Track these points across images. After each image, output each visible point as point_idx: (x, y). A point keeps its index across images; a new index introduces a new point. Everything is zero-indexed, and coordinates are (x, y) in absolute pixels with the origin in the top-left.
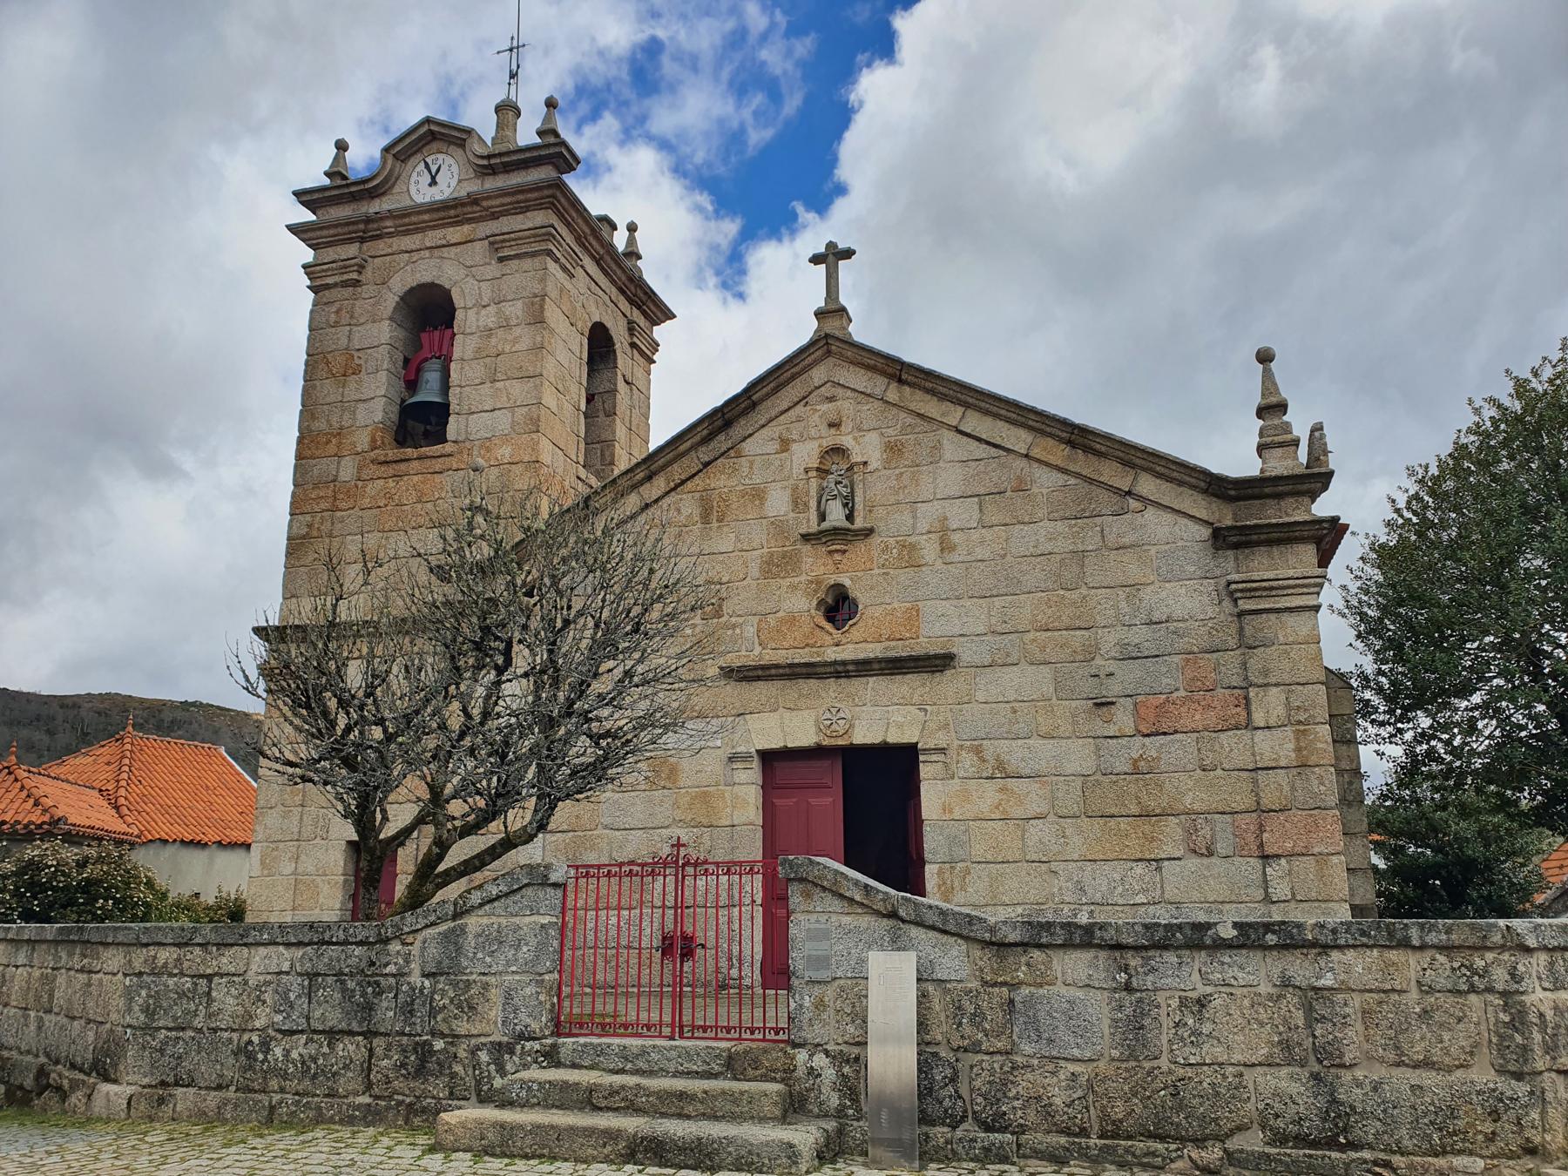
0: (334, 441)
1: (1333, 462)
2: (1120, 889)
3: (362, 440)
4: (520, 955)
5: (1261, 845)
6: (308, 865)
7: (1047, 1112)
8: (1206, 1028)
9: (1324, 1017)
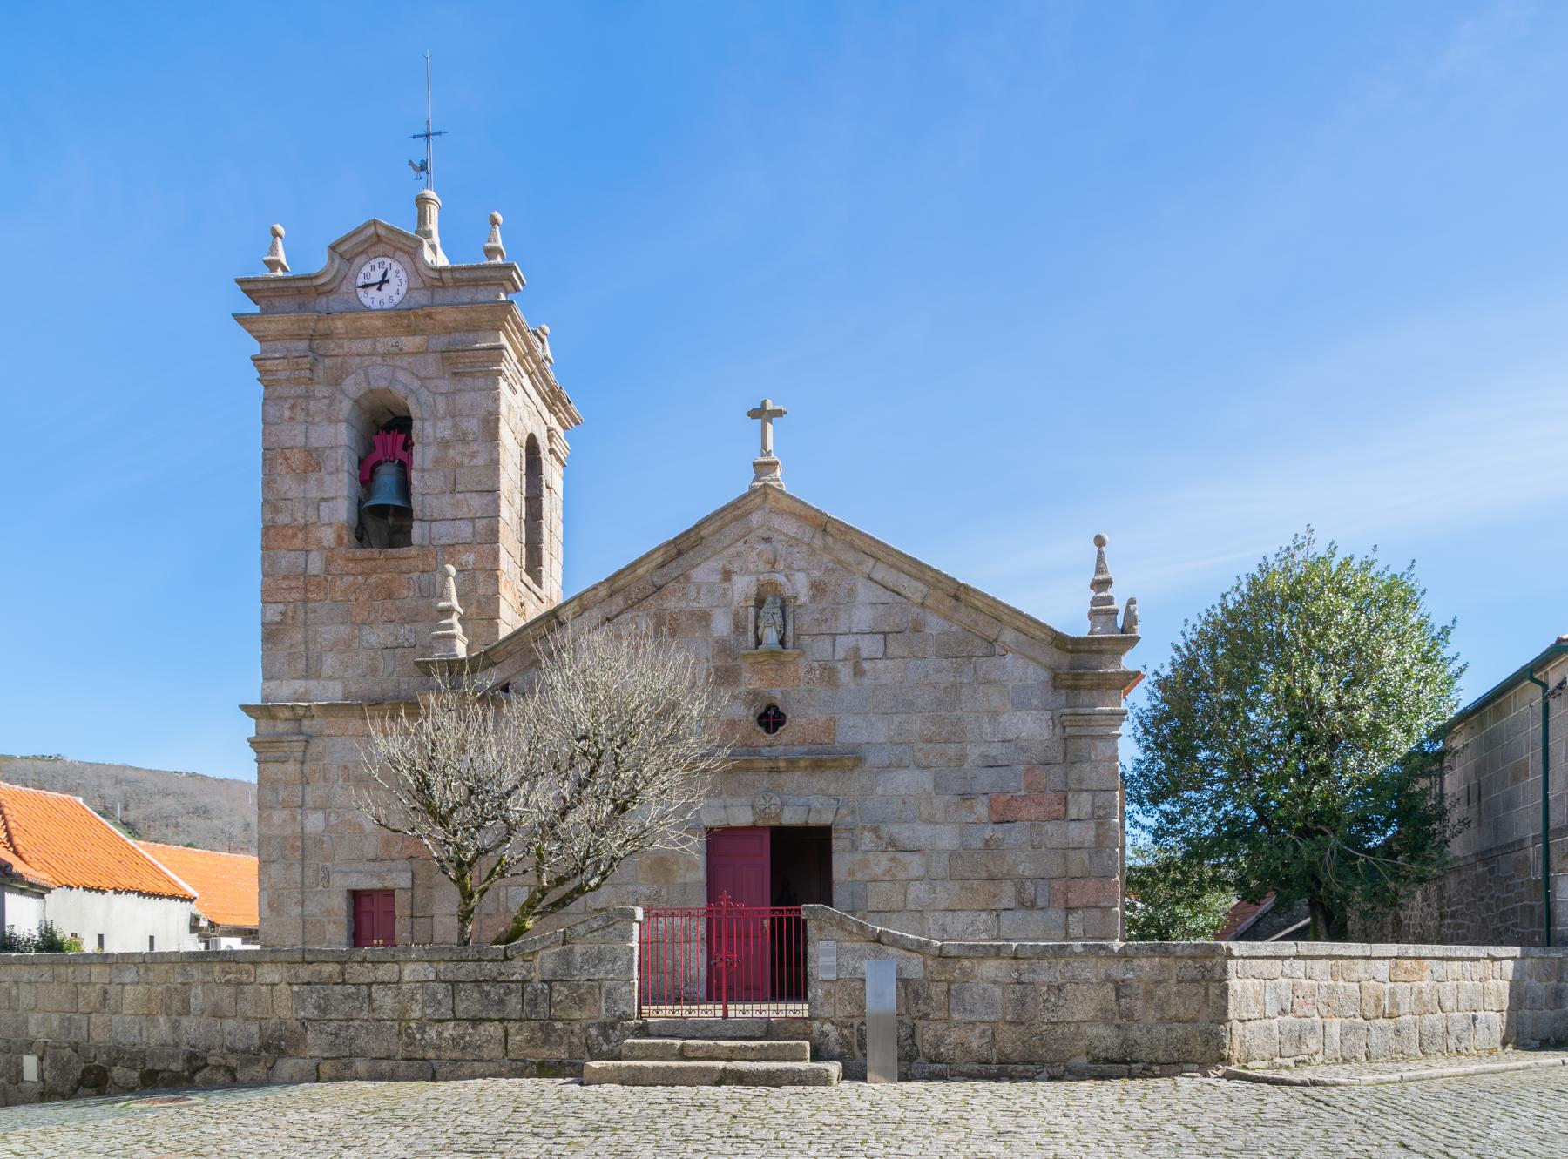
0: (300, 535)
1: (1139, 630)
2: (970, 930)
3: (328, 536)
4: (616, 967)
5: (1066, 901)
6: (312, 909)
7: (968, 1051)
8: (1062, 1002)
9: (929, 1107)
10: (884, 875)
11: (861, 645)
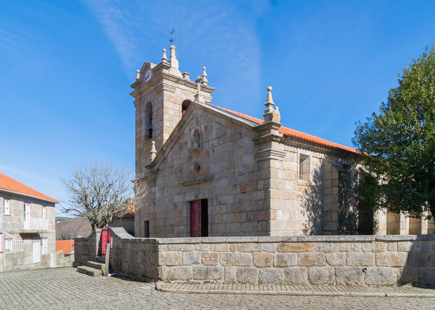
10: (218, 212)
11: (214, 143)
